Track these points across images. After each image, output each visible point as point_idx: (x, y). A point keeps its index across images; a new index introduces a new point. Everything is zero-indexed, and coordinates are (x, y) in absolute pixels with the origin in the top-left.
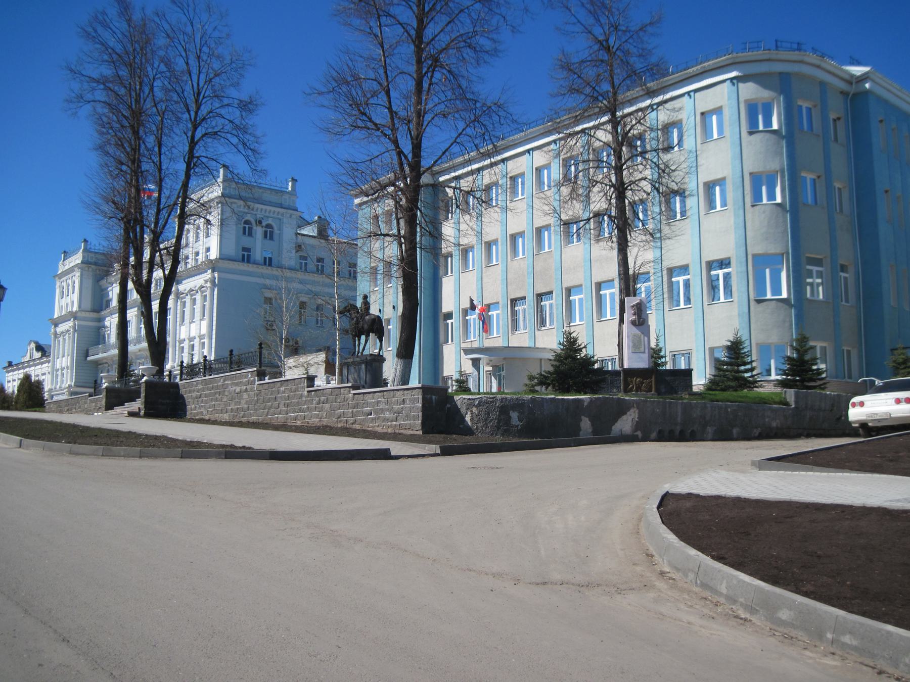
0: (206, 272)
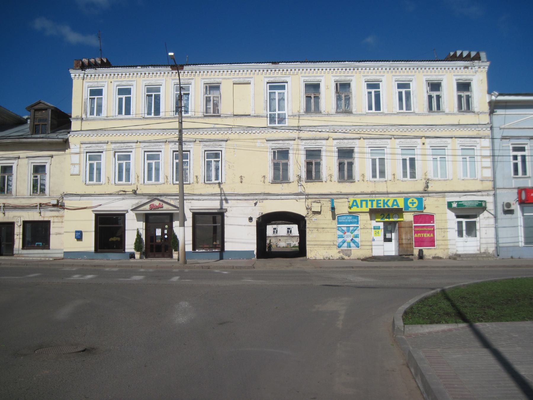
0: (70, 81)
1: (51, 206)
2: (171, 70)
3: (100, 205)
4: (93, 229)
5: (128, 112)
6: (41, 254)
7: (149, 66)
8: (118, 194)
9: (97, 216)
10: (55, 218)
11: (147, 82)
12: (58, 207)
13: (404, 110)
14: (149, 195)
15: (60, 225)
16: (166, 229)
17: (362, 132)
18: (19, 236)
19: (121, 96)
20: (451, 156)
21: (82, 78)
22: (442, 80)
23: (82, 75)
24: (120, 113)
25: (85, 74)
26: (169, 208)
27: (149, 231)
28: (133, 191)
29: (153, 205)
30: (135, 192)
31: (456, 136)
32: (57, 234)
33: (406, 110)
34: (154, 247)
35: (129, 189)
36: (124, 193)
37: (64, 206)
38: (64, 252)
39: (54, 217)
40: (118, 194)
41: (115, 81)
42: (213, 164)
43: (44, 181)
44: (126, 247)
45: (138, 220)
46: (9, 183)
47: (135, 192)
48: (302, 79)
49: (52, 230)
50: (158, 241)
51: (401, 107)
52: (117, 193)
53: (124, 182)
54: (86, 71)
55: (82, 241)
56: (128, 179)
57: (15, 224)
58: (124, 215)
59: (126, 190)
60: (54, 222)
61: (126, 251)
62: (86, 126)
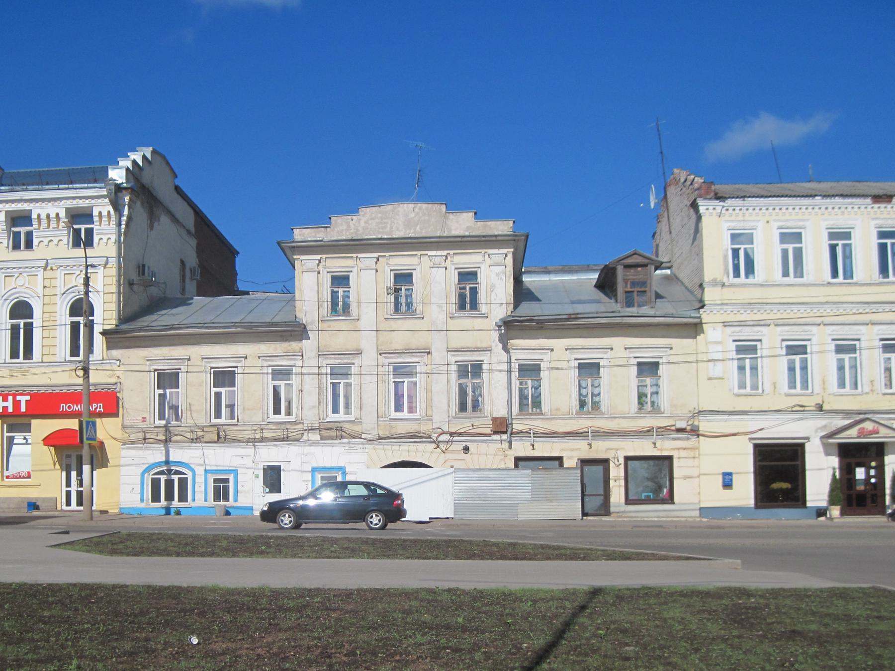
0: (201, 276)
1: (673, 431)
2: (871, 203)
3: (761, 430)
4: (751, 468)
5: (799, 273)
6: (660, 511)
7: (837, 196)
8: (793, 411)
9: (756, 446)
10: (681, 451)
11: (830, 223)
12: (686, 432)
13: (841, 278)
14: (847, 413)
15: (690, 462)
16: (872, 468)
17: (825, 314)
18: (618, 481)
19: (785, 246)
20: (768, 359)
21: (719, 214)
22: (853, 228)
23: (719, 209)
24: (786, 274)
25: (723, 207)
26: (888, 434)
27: (847, 470)
28: (818, 406)
29: (863, 428)
30: (820, 408)
31: (873, 322)
32: (686, 478)
33: (845, 278)
34: (854, 496)
35: (810, 402)
36: (802, 409)
37: (698, 431)
38: (701, 509)
39: (678, 449)
40: (793, 411)
41: (775, 221)
42: (748, 363)
43: (645, 388)
44: (808, 498)
45: (827, 454)
46: (581, 392)
47: (820, 408)
48: (873, 223)
49: (678, 471)
50: (861, 487)
51: (835, 274)
52: (790, 409)
53: (798, 389)
54: (726, 202)
55: (732, 489)
56: (805, 384)
57: (611, 462)
58: (802, 446)
59: (804, 404)
60: (679, 458)
61: (809, 504)
62: (728, 295)
